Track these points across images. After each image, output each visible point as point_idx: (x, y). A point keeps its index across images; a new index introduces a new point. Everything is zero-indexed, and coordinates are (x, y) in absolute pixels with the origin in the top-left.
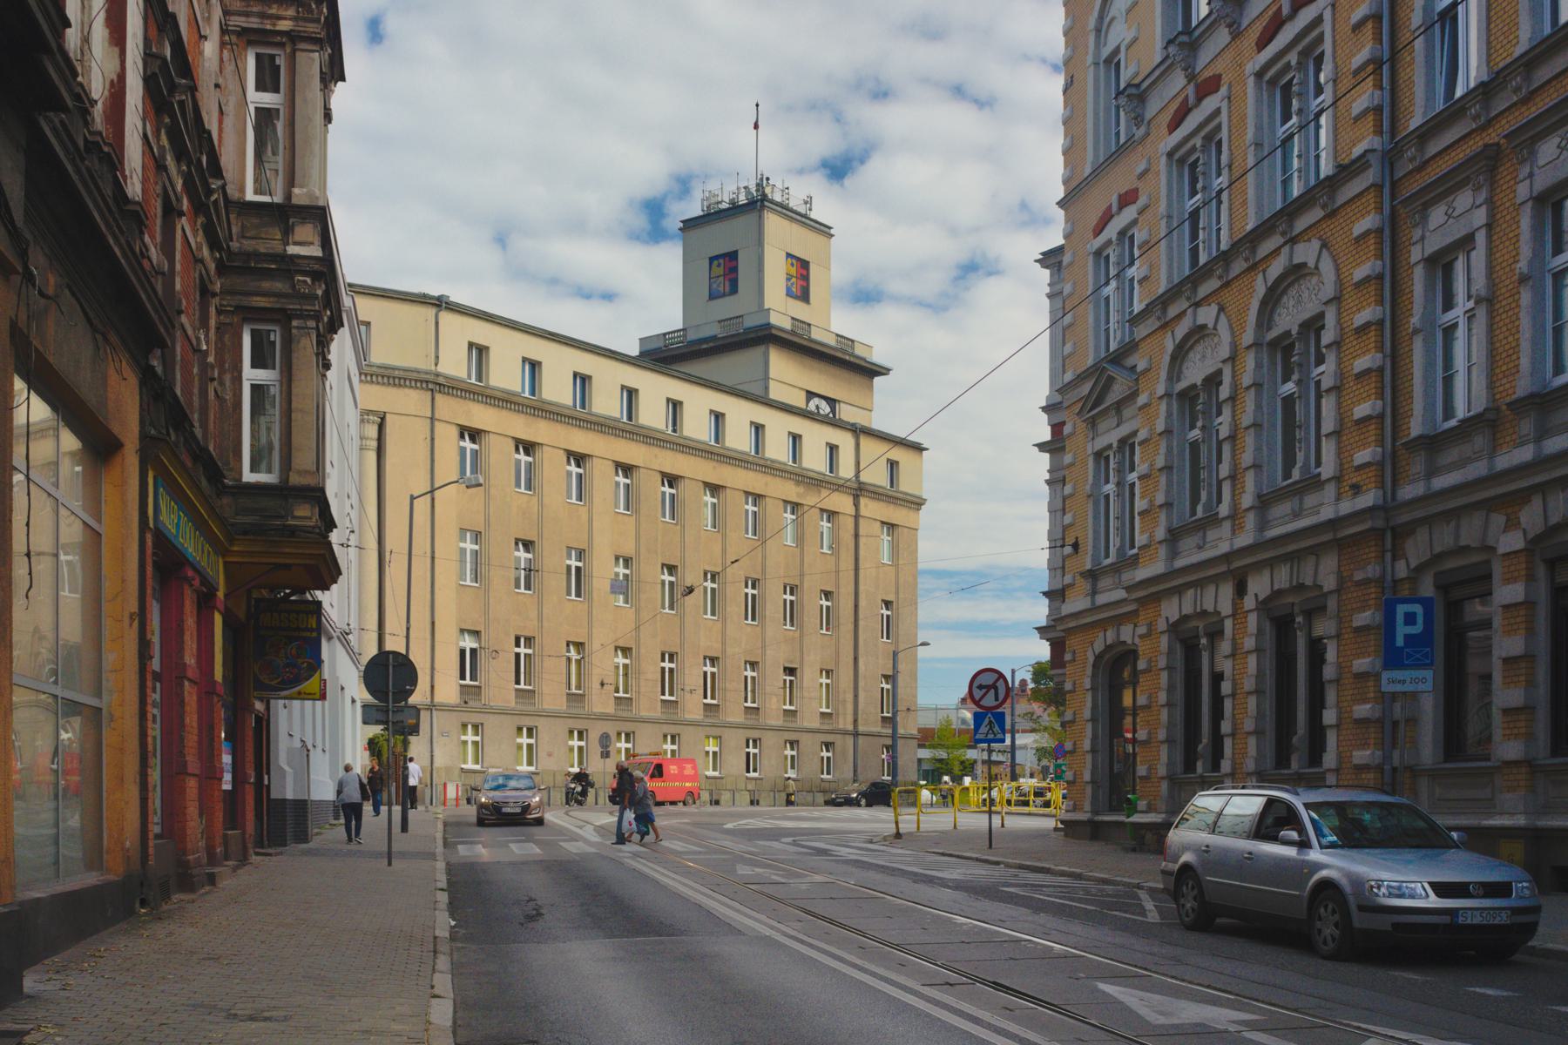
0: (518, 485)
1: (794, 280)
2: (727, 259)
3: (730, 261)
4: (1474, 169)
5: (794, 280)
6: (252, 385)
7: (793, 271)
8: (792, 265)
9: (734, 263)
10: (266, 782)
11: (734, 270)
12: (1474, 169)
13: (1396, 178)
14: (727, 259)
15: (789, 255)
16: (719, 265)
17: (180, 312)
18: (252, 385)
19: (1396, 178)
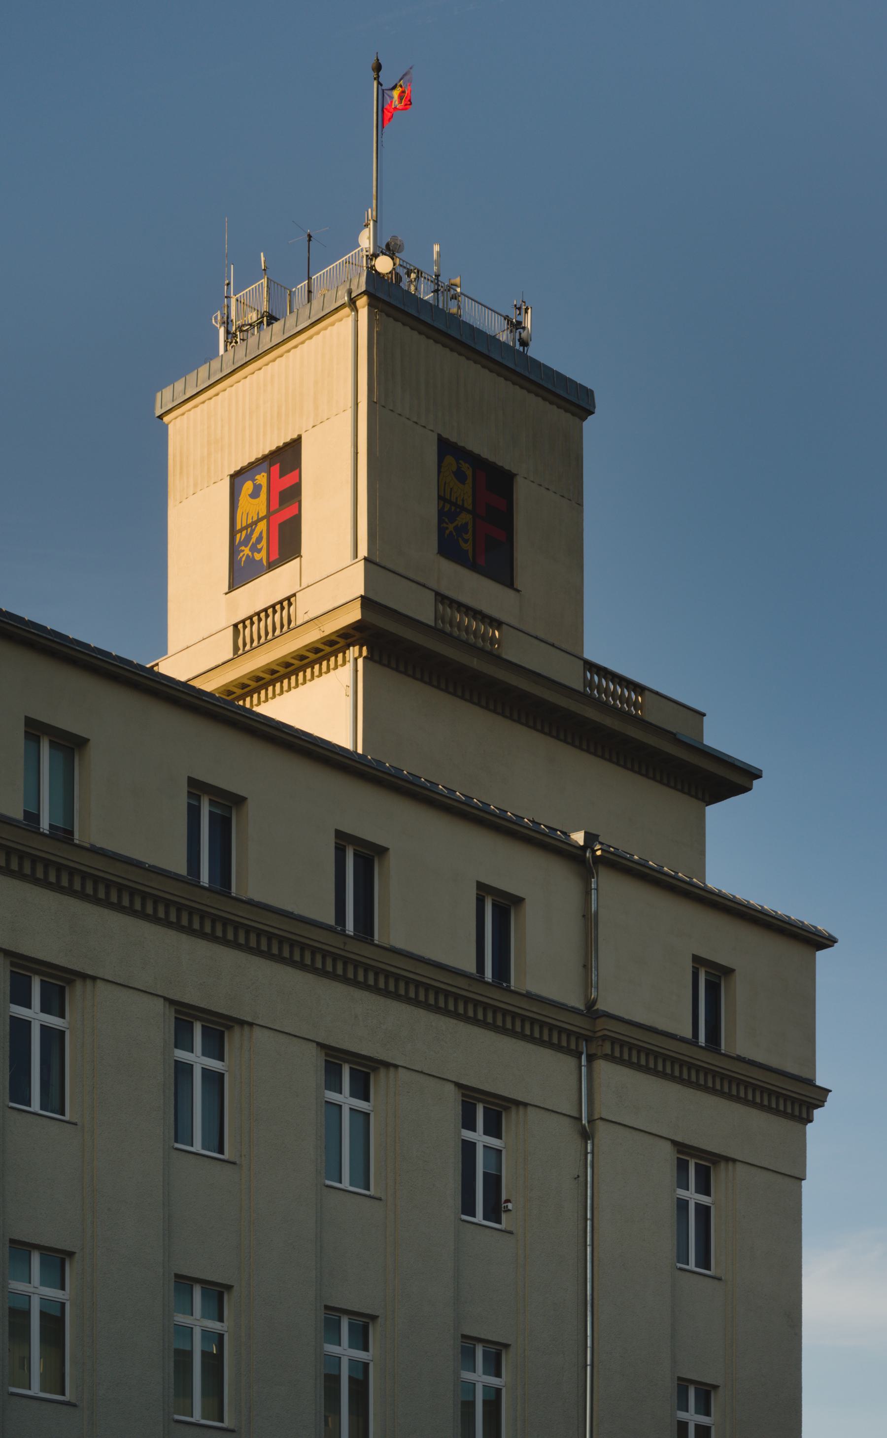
0: (468, 1208)
1: (465, 518)
2: (276, 468)
3: (282, 474)
4: (394, 278)
5: (465, 518)
6: (695, 1424)
7: (464, 493)
8: (460, 476)
9: (288, 481)
10: (42, 1360)
11: (293, 494)
12: (394, 278)
13: (352, 297)
14: (276, 468)
15: (446, 447)
16: (255, 494)
17: (336, 928)
18: (695, 1424)
19: (352, 297)
